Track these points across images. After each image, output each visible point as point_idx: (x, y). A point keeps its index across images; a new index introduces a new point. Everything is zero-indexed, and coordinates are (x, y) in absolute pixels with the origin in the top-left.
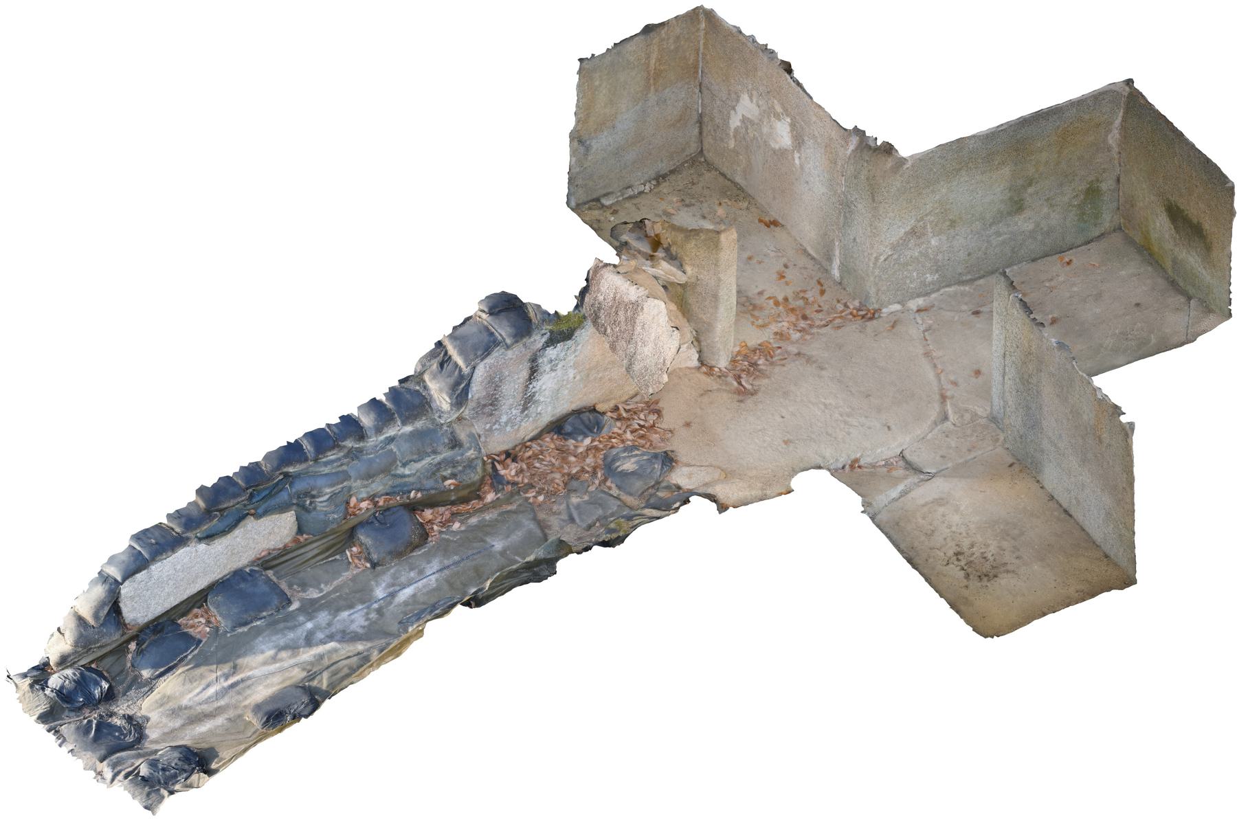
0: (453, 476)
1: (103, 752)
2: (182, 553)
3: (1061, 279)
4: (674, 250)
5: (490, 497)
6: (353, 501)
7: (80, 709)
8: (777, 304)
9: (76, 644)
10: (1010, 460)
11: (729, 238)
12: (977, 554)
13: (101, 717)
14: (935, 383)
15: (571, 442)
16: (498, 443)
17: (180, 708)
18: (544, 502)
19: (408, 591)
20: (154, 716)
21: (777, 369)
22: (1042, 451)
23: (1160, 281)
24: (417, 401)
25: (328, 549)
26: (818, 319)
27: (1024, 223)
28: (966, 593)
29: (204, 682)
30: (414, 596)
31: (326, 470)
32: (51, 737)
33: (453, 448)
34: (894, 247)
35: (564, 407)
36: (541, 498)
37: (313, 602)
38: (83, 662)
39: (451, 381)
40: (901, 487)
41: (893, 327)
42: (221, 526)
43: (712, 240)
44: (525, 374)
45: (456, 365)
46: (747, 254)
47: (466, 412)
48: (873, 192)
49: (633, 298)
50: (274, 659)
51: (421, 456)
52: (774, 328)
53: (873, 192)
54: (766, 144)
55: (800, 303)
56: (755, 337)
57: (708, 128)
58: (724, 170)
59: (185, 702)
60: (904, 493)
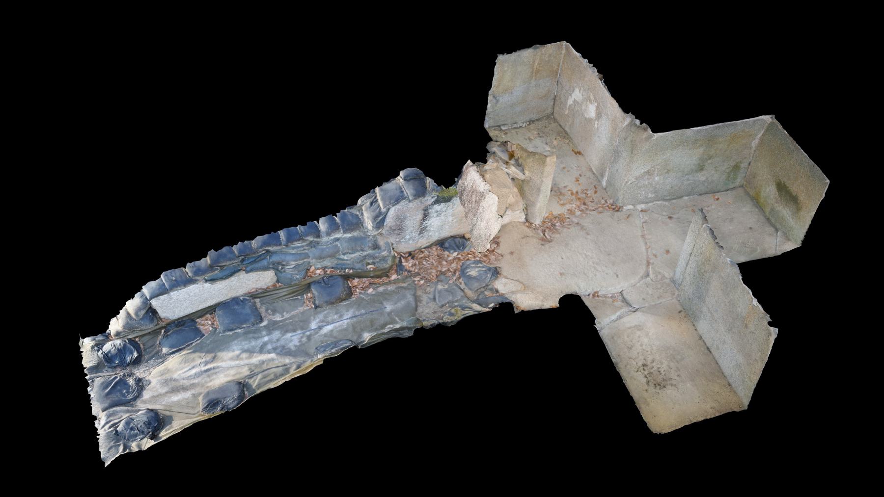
0: (374, 263)
1: (106, 405)
2: (192, 288)
3: (713, 207)
4: (520, 161)
5: (394, 277)
6: (313, 268)
7: (115, 367)
8: (572, 194)
9: (124, 327)
10: (680, 308)
11: (551, 161)
12: (655, 368)
13: (124, 375)
14: (645, 254)
16: (404, 248)
17: (171, 380)
18: (423, 285)
20: (154, 382)
21: (565, 230)
22: (701, 312)
23: (762, 217)
24: (355, 221)
25: (293, 293)
26: (591, 206)
27: (701, 177)
28: (645, 395)
29: (193, 364)
30: (332, 331)
31: (294, 252)
33: (374, 249)
34: (636, 178)
35: (446, 233)
36: (422, 282)
37: (275, 323)
38: (130, 337)
39: (374, 214)
40: (618, 313)
42: (220, 275)
43: (542, 159)
44: (420, 216)
45: (379, 206)
46: (562, 166)
47: (383, 231)
48: (633, 149)
49: (481, 190)
50: (238, 357)
51: (354, 251)
52: (568, 207)
53: (633, 149)
54: (583, 115)
55: (584, 196)
56: (558, 210)
57: (558, 102)
58: (561, 123)
59: (175, 376)
60: (620, 318)
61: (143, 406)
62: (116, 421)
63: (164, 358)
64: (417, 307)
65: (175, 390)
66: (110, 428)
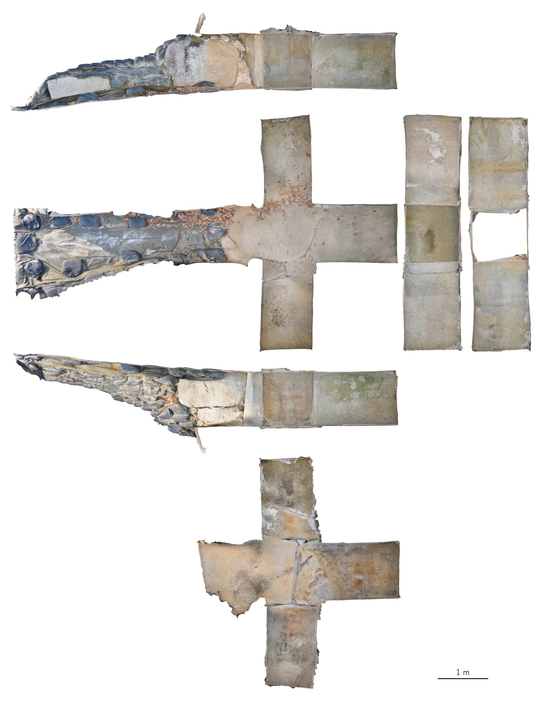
1: (21, 252)
3: (369, 217)
8: (290, 187)
15: (203, 215)
17: (52, 244)
19: (132, 241)
21: (274, 213)
29: (63, 240)
30: (133, 243)
32: (14, 235)
36: (186, 226)
37: (107, 229)
41: (313, 213)
46: (295, 163)
50: (85, 243)
52: (283, 197)
59: (54, 243)
61: (38, 256)
62: (24, 261)
63: (51, 230)
64: (178, 241)
65: (54, 251)
66: (21, 265)
